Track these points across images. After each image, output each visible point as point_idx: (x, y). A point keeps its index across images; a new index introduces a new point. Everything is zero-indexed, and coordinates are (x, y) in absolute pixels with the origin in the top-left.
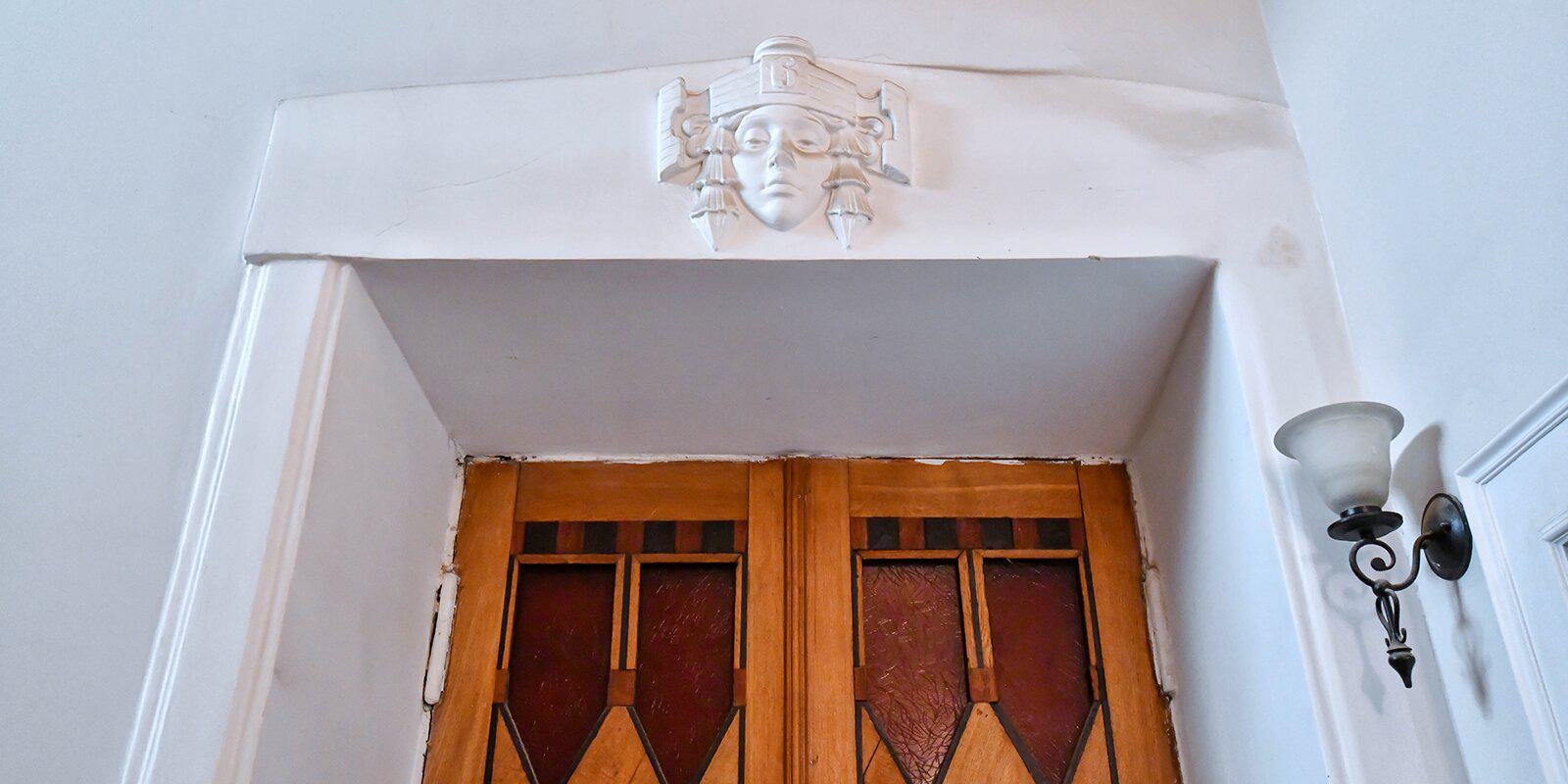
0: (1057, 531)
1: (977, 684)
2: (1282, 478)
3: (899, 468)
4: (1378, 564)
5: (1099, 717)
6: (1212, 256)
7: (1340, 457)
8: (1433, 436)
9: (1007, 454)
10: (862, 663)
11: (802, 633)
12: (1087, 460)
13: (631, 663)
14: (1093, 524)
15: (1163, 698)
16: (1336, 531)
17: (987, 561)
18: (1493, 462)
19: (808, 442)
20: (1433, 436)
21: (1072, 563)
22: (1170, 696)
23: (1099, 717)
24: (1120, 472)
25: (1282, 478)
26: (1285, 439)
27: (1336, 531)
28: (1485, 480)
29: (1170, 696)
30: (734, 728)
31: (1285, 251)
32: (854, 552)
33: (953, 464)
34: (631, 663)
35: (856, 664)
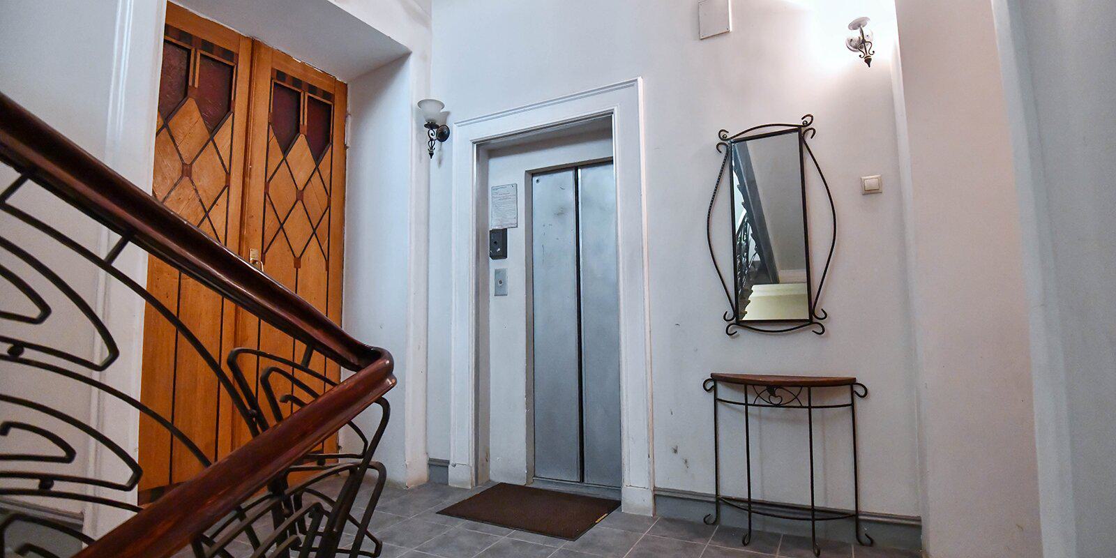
0: (327, 95)
1: (301, 129)
2: (414, 109)
3: (288, 58)
4: (432, 134)
5: (330, 148)
6: (411, 50)
7: (432, 112)
8: (448, 113)
9: (319, 67)
10: (271, 111)
11: (254, 100)
12: (338, 79)
13: (196, 86)
14: (337, 97)
15: (346, 147)
16: (426, 126)
17: (309, 97)
18: (460, 124)
19: (262, 37)
20: (448, 113)
21: (330, 106)
22: (347, 147)
23: (330, 148)
24: (346, 85)
25: (414, 109)
26: (420, 104)
27: (426, 126)
28: (459, 126)
29: (347, 147)
30: (230, 120)
31: (425, 58)
32: (272, 79)
33: (303, 64)
34: (196, 86)
35: (269, 112)
